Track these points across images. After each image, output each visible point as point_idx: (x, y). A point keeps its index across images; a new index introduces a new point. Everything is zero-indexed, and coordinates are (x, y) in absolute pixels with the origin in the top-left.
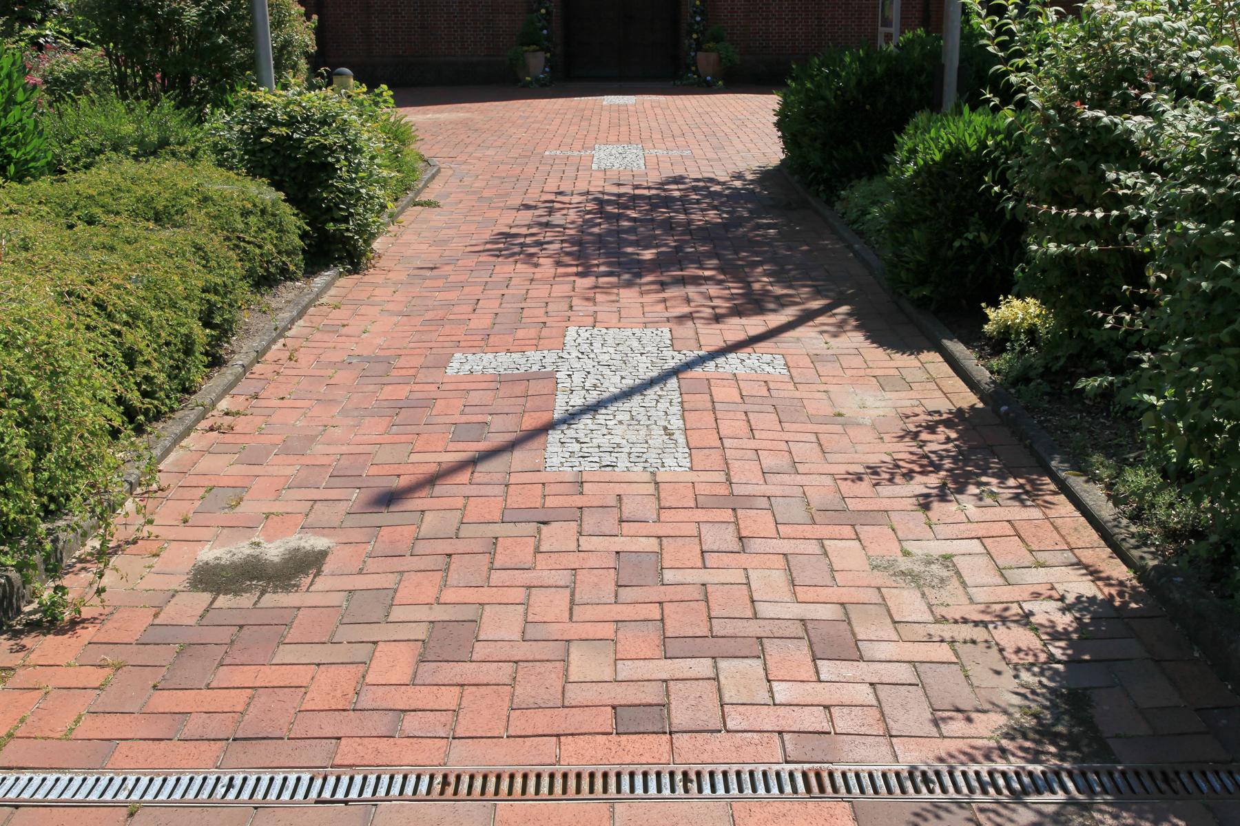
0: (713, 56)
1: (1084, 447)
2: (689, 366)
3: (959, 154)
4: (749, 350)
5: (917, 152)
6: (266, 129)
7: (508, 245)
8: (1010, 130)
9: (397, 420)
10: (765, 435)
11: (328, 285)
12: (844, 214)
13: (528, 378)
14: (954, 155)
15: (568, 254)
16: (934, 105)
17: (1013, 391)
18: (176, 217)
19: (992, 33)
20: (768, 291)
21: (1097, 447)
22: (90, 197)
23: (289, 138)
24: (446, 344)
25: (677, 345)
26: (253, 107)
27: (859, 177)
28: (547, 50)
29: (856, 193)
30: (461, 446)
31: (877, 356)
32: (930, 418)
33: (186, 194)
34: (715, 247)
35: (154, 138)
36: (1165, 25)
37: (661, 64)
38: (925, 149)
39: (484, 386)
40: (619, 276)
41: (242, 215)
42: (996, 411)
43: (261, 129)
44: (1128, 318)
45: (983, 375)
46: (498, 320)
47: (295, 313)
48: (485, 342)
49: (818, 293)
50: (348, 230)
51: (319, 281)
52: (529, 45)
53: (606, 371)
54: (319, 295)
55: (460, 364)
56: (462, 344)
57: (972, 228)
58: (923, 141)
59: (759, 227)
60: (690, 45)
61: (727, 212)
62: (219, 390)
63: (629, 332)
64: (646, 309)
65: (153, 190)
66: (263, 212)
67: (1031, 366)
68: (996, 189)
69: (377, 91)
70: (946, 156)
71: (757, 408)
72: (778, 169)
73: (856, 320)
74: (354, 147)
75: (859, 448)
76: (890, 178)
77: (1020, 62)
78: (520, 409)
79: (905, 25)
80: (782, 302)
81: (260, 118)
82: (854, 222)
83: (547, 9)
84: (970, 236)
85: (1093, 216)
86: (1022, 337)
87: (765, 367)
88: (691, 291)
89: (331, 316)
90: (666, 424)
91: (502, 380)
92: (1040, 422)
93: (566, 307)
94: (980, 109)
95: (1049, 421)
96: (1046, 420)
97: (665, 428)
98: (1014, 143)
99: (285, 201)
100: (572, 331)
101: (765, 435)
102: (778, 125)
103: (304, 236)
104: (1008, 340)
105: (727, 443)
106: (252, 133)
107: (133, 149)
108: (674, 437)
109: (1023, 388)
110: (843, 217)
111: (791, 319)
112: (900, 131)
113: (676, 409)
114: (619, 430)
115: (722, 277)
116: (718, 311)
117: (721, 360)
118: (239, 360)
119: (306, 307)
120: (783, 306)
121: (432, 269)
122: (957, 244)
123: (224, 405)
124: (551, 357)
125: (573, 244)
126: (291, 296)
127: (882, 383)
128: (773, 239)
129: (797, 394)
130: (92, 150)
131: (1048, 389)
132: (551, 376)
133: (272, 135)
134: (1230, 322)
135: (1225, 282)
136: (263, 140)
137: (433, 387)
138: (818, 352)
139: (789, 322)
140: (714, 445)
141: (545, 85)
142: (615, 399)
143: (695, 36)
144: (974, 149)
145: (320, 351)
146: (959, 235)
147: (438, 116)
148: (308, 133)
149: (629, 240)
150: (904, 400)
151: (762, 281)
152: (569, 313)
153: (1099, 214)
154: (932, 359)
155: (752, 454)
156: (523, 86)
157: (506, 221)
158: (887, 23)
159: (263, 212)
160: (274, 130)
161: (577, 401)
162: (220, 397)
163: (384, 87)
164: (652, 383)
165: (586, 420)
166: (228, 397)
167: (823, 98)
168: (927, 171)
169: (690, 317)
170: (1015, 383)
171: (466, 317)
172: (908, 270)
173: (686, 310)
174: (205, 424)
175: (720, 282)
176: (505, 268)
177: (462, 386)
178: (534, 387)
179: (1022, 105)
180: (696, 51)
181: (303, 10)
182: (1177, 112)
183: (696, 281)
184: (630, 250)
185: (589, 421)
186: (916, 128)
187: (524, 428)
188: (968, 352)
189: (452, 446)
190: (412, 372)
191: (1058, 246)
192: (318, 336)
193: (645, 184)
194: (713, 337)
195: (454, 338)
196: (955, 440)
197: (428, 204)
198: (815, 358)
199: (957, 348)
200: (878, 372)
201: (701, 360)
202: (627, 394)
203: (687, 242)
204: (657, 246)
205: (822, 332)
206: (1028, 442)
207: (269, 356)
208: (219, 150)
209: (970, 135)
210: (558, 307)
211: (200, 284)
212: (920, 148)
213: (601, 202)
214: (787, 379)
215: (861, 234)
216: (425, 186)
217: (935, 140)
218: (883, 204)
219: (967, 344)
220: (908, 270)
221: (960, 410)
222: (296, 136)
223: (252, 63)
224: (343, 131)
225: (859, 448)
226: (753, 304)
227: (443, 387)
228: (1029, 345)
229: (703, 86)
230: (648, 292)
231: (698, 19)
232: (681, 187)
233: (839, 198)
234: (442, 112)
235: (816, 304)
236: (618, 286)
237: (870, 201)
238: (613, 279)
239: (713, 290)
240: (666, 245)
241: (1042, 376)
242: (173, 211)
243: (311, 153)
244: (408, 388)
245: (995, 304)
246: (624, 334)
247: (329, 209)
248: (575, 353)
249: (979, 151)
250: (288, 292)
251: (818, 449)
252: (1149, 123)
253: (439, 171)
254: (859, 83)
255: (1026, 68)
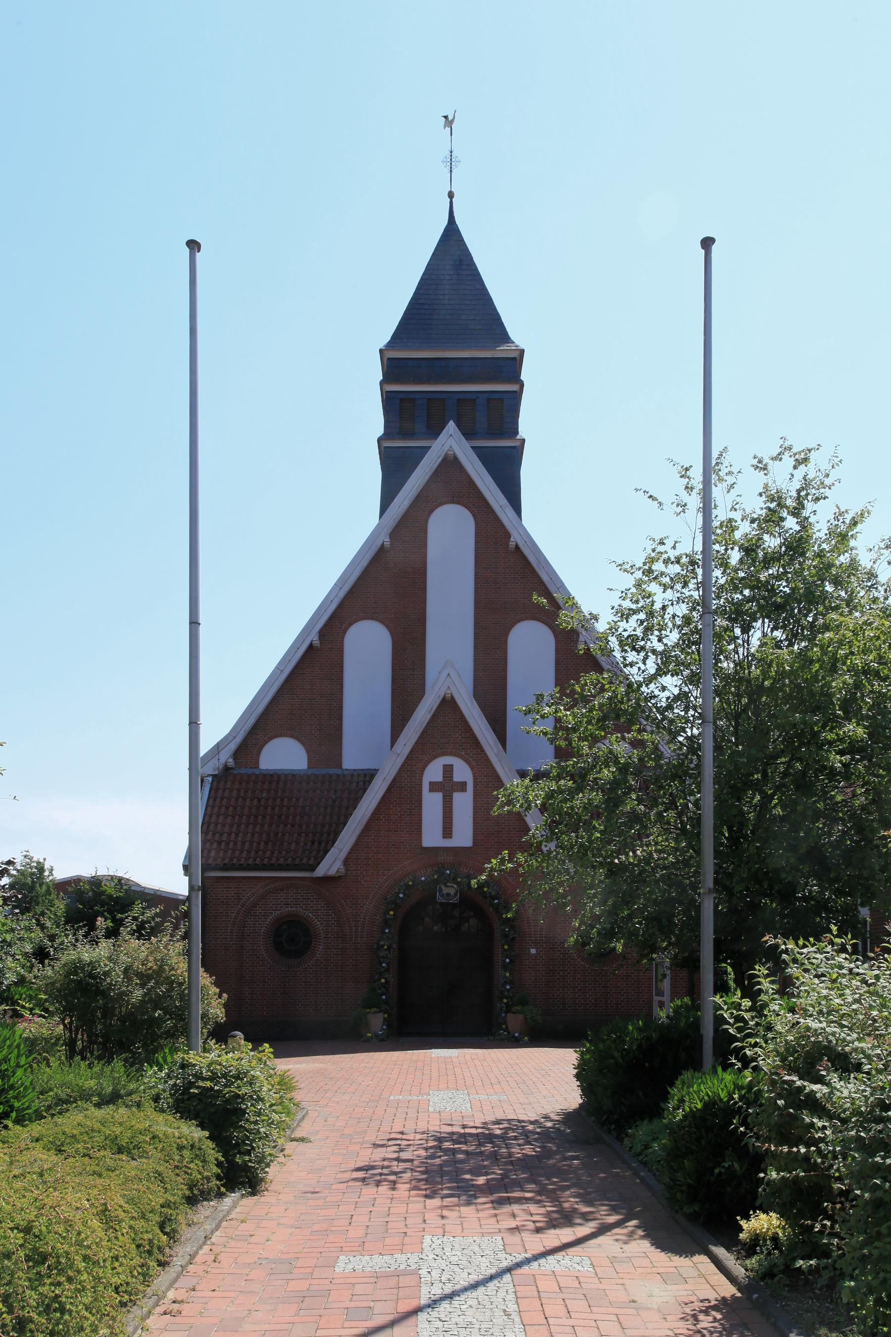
0: (520, 1017)
1: (813, 1324)
2: (519, 1265)
3: (715, 1103)
4: (563, 1253)
5: (684, 1101)
6: (194, 1083)
7: (370, 1175)
8: (750, 1086)
9: (304, 1306)
10: (578, 1315)
11: (235, 1205)
12: (631, 1148)
13: (397, 1274)
14: (711, 1105)
15: (420, 1180)
16: (696, 1065)
17: (762, 1284)
18: (133, 1151)
19: (732, 1021)
20: (576, 1209)
21: (822, 1323)
22: (74, 1136)
23: (212, 1089)
24: (332, 1249)
25: (509, 1250)
26: (183, 1066)
27: (642, 1119)
28: (386, 1012)
29: (641, 1131)
30: (353, 1324)
31: (660, 1258)
32: (701, 1304)
33: (140, 1133)
34: (532, 1175)
35: (109, 1090)
36: (827, 1029)
37: (480, 1027)
38: (690, 1099)
39: (365, 1280)
40: (459, 1197)
41: (178, 1149)
42: (749, 1298)
43: (190, 1082)
44: (829, 1224)
45: (739, 1271)
46: (369, 1231)
47: (214, 1226)
48: (362, 1248)
49: (614, 1210)
50: (250, 1161)
51: (228, 1201)
52: (370, 1008)
53: (456, 1269)
54: (229, 1212)
55: (344, 1264)
56: (344, 1249)
57: (727, 1159)
58: (689, 1093)
59: (566, 1159)
60: (501, 1008)
61: (539, 1147)
62: (167, 1284)
63: (470, 1240)
64: (482, 1222)
65: (118, 1130)
66: (192, 1146)
67: (775, 1264)
68: (742, 1129)
69: (260, 1049)
70: (706, 1105)
71: (572, 1296)
72: (576, 1111)
73: (644, 1231)
74: (258, 1096)
75: (649, 1325)
76: (665, 1121)
77: (752, 1041)
78: (394, 1297)
79: (674, 995)
80: (586, 1217)
81: (189, 1075)
82: (639, 1154)
83: (386, 979)
84: (726, 1165)
85: (799, 1151)
86: (768, 1242)
87: (575, 1265)
88: (516, 1208)
89: (240, 1228)
90: (505, 1308)
91: (377, 1277)
92: (783, 1306)
93: (421, 1221)
94: (729, 1070)
95: (789, 1305)
96: (786, 1305)
97: (505, 1311)
98: (751, 1096)
99: (207, 1138)
100: (427, 1239)
101: (578, 1315)
102: (578, 1076)
103: (219, 1164)
104: (758, 1245)
105: (551, 1321)
106: (183, 1086)
107: (95, 1099)
108: (511, 1317)
109: (769, 1281)
110: (630, 1151)
111: (594, 1230)
112: (672, 1085)
113: (511, 1296)
114: (469, 1312)
115: (539, 1198)
116: (538, 1225)
117: (542, 1261)
118: (178, 1261)
119: (221, 1222)
120: (588, 1220)
121: (313, 1193)
122: (717, 1171)
123: (171, 1295)
124: (413, 1259)
125: (422, 1173)
126: (208, 1213)
127: (665, 1278)
128: (577, 1169)
129: (601, 1286)
130: (60, 1100)
131: (788, 1282)
132: (416, 1273)
133: (198, 1087)
134: (888, 1221)
135: (879, 1194)
136: (192, 1091)
137: (327, 1282)
138: (616, 1255)
139: (593, 1233)
140: (541, 1323)
141: (383, 1040)
142: (466, 1289)
143: (505, 1001)
144: (725, 1100)
145: (237, 1255)
146: (719, 1165)
147: (298, 1066)
148: (225, 1086)
149: (464, 1167)
150: (682, 1291)
151: (570, 1201)
152: (424, 1225)
153: (803, 1150)
154: (702, 1260)
155: (570, 1329)
156: (365, 1041)
157: (367, 1156)
158: (660, 993)
159: (192, 1146)
160: (201, 1084)
161: (437, 1291)
162: (168, 1289)
163: (267, 1045)
164: (492, 1278)
165: (445, 1304)
166: (173, 1290)
167: (612, 1058)
168: (692, 1115)
169: (517, 1229)
170: (763, 1278)
171: (345, 1228)
172: (681, 1191)
173: (513, 1224)
174: (159, 1310)
175: (538, 1202)
176: (370, 1191)
177: (349, 1281)
178: (403, 1281)
179: (756, 1069)
180: (506, 1013)
181: (218, 990)
182: (842, 1083)
183: (519, 1201)
184: (468, 1177)
185: (448, 1306)
186: (683, 1083)
187: (399, 1311)
188: (729, 1255)
189: (346, 1324)
190: (310, 1270)
191: (778, 1174)
192: (232, 1243)
193: (472, 1124)
194: (536, 1243)
195: (337, 1245)
196: (720, 1320)
197: (302, 1140)
198: (613, 1260)
199: (720, 1251)
200: (661, 1270)
201: (528, 1261)
202: (474, 1286)
203: (510, 1171)
204: (486, 1174)
205: (617, 1240)
206: (773, 1320)
207: (199, 1259)
208: (156, 1099)
209: (722, 1089)
210: (414, 1221)
211: (161, 1201)
212: (687, 1099)
213: (440, 1140)
214: (593, 1275)
215: (645, 1164)
216: (298, 1125)
217: (698, 1092)
218: (661, 1140)
219: (728, 1249)
220: (681, 1191)
221: (723, 1298)
222: (216, 1088)
223: (186, 1031)
224: (251, 1084)
225: (649, 1325)
226: (565, 1219)
227: (334, 1281)
228: (774, 1249)
229: (514, 1042)
230: (483, 1210)
231: (508, 987)
232: (501, 1126)
233: (627, 1135)
234: (301, 1063)
235: (612, 1219)
236: (459, 1205)
237: (651, 1139)
238: (455, 1199)
239: (533, 1208)
240: (494, 1173)
241: (783, 1272)
242: (131, 1147)
243: (227, 1101)
244: (308, 1282)
245: (747, 1217)
246: (468, 1240)
247: (237, 1144)
248: (432, 1256)
249: (729, 1101)
250: (206, 1209)
251: (619, 1326)
252: (826, 1090)
253: (307, 1113)
254: (640, 1046)
255: (756, 1045)
